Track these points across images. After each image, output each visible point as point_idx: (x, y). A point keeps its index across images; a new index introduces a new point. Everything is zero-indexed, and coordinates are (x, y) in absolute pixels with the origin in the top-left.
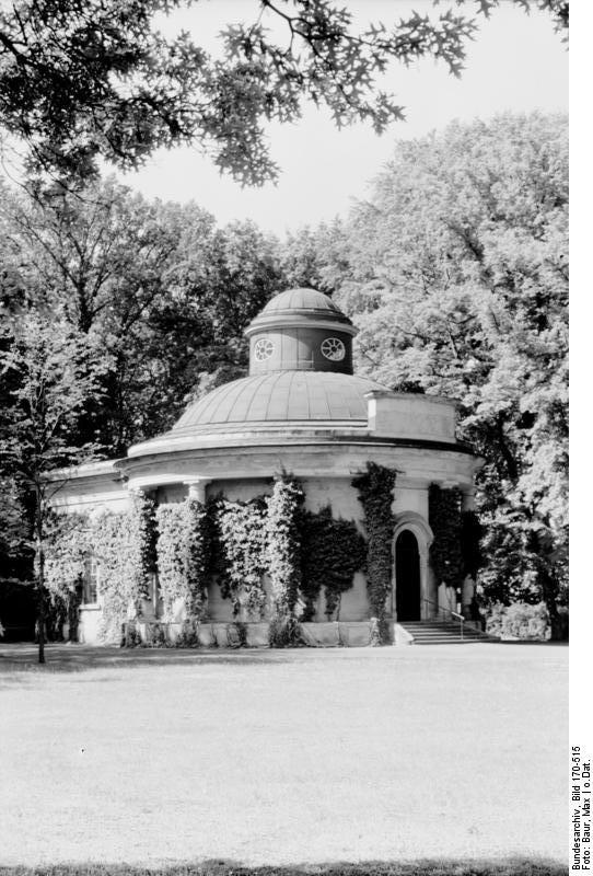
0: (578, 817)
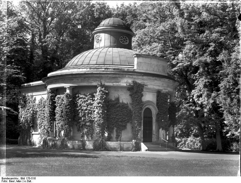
0: (16, 179)
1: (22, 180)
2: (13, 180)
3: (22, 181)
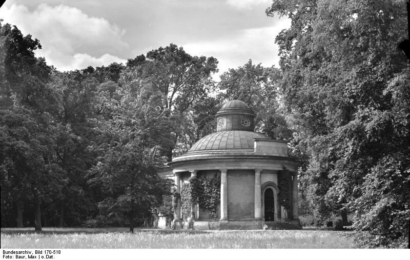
0: (27, 253)
1: (37, 255)
2: (22, 255)
3: (37, 257)
